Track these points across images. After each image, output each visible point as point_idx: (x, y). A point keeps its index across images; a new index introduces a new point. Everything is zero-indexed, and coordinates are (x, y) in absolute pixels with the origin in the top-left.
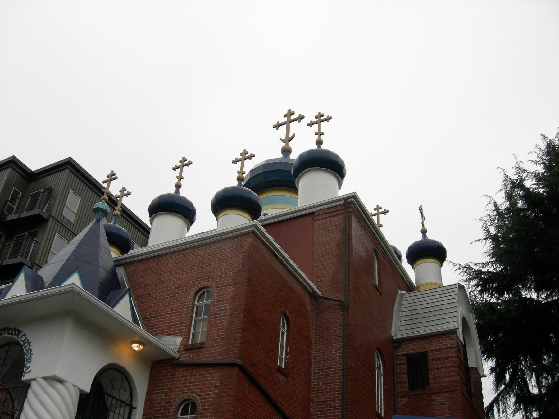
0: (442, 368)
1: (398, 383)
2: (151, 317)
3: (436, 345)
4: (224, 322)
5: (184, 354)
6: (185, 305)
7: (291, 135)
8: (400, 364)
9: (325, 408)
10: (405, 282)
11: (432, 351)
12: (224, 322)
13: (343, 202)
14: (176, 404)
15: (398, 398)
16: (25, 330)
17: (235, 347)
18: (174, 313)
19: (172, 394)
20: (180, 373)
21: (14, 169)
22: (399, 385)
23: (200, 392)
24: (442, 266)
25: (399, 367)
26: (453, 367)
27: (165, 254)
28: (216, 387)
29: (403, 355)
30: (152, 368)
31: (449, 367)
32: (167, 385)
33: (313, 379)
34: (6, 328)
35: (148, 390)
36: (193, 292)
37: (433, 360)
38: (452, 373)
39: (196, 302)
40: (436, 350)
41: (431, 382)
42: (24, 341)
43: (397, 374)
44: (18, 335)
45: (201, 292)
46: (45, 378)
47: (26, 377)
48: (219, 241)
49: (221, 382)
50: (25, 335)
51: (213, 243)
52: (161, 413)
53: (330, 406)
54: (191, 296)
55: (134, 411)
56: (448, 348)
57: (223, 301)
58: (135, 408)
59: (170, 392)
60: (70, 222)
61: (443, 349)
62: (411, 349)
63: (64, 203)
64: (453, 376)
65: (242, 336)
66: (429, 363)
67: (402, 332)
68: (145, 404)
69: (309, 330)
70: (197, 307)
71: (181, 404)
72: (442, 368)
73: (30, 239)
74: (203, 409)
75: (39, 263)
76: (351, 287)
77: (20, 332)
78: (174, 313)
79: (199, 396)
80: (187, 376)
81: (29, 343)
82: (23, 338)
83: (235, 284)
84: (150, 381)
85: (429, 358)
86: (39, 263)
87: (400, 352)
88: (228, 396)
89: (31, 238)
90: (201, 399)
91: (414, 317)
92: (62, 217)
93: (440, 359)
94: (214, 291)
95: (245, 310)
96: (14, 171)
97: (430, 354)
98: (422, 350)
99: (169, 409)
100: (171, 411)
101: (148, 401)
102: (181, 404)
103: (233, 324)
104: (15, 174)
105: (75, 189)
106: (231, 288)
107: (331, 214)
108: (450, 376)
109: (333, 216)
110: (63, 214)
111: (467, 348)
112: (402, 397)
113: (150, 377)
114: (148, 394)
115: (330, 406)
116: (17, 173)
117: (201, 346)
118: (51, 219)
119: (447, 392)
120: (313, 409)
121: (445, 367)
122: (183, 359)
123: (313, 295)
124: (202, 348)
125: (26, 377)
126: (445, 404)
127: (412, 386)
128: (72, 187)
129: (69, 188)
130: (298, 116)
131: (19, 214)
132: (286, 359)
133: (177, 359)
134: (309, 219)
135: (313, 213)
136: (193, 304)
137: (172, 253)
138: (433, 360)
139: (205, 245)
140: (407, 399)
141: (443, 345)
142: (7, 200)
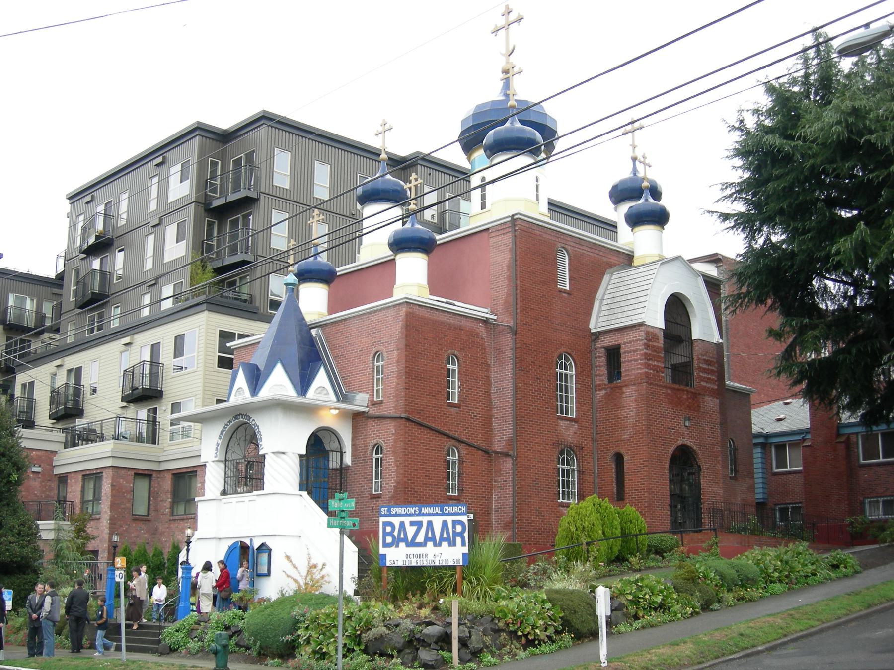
0: (631, 361)
1: (596, 376)
2: (347, 376)
3: (628, 337)
4: (393, 382)
5: (372, 408)
6: (367, 367)
7: (511, 48)
8: (600, 357)
9: (502, 423)
10: (623, 253)
11: (625, 343)
12: (393, 382)
13: (509, 219)
14: (370, 448)
15: (596, 390)
16: (253, 417)
17: (401, 403)
18: (361, 373)
19: (368, 439)
20: (371, 423)
21: (203, 136)
22: (598, 378)
23: (384, 438)
24: (664, 229)
25: (598, 359)
26: (641, 360)
27: (349, 318)
28: (393, 434)
29: (602, 347)
30: (353, 419)
31: (637, 360)
32: (363, 433)
33: (494, 398)
34: (240, 414)
35: (352, 437)
36: (372, 355)
37: (625, 352)
38: (640, 366)
39: (376, 363)
40: (628, 343)
41: (623, 374)
42: (254, 425)
43: (596, 367)
44: (249, 420)
45: (377, 355)
46: (273, 453)
47: (261, 452)
48: (384, 309)
49: (396, 431)
50: (254, 420)
51: (381, 310)
52: (363, 455)
53: (506, 421)
54: (371, 358)
55: (344, 455)
56: (637, 340)
57: (391, 364)
58: (345, 452)
59: (366, 438)
60: (285, 190)
61: (633, 341)
62: (608, 341)
63: (271, 170)
64: (640, 369)
65: (406, 394)
66: (622, 355)
67: (600, 325)
68: (352, 448)
69: (485, 356)
70: (377, 367)
71: (374, 447)
72: (631, 361)
73: (248, 166)
74: (387, 451)
75: (263, 253)
76: (518, 311)
77: (250, 418)
78: (361, 373)
79: (383, 441)
80: (374, 426)
81: (258, 427)
82: (253, 423)
83: (398, 350)
84: (352, 429)
85: (622, 351)
86: (263, 253)
87: (599, 345)
88: (401, 441)
89: (246, 229)
90: (385, 443)
91: (613, 306)
92: (275, 187)
93: (630, 352)
94: (385, 354)
95: (406, 372)
96: (204, 138)
97: (623, 346)
98: (617, 343)
99: (366, 451)
100: (368, 452)
101: (354, 445)
102: (374, 447)
103: (399, 384)
104: (206, 143)
105: (280, 147)
106: (395, 353)
107: (502, 232)
108: (638, 368)
109: (504, 234)
110: (274, 184)
111: (691, 318)
112: (600, 390)
113: (352, 427)
114: (353, 440)
115: (506, 421)
116: (208, 139)
117: (381, 402)
118: (262, 196)
119: (634, 384)
120: (495, 423)
121: (635, 360)
122: (371, 412)
123: (486, 321)
124: (382, 403)
125: (261, 452)
126: (633, 396)
127: (611, 378)
128: (276, 145)
129: (272, 148)
130: (517, 15)
131: (225, 198)
132: (458, 392)
133: (367, 413)
134: (485, 234)
135: (488, 229)
136: (373, 365)
137: (354, 317)
138: (625, 352)
139: (375, 311)
140: (604, 392)
141: (633, 338)
142: (205, 179)
